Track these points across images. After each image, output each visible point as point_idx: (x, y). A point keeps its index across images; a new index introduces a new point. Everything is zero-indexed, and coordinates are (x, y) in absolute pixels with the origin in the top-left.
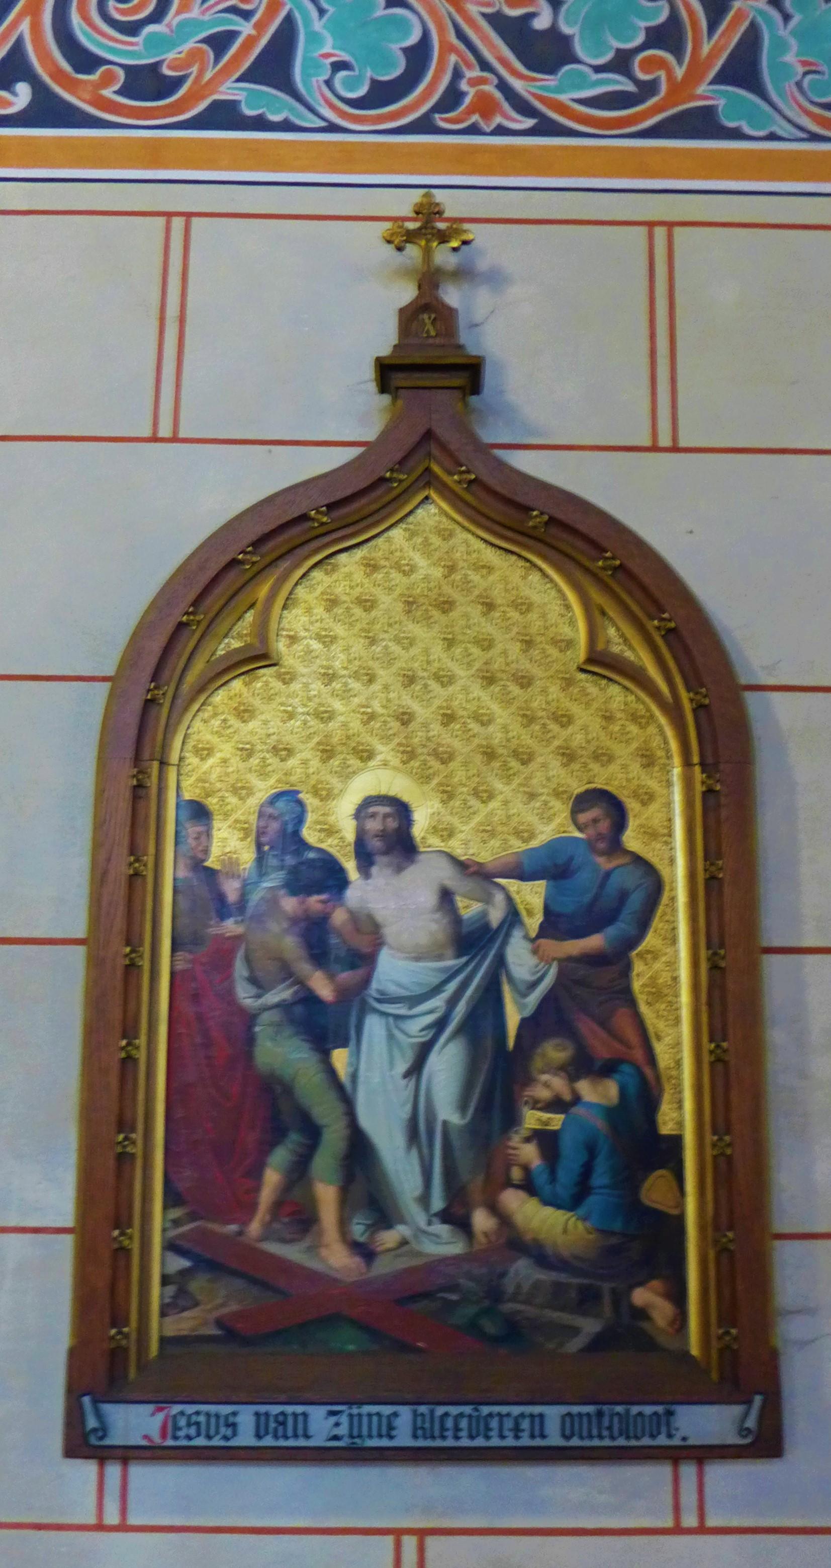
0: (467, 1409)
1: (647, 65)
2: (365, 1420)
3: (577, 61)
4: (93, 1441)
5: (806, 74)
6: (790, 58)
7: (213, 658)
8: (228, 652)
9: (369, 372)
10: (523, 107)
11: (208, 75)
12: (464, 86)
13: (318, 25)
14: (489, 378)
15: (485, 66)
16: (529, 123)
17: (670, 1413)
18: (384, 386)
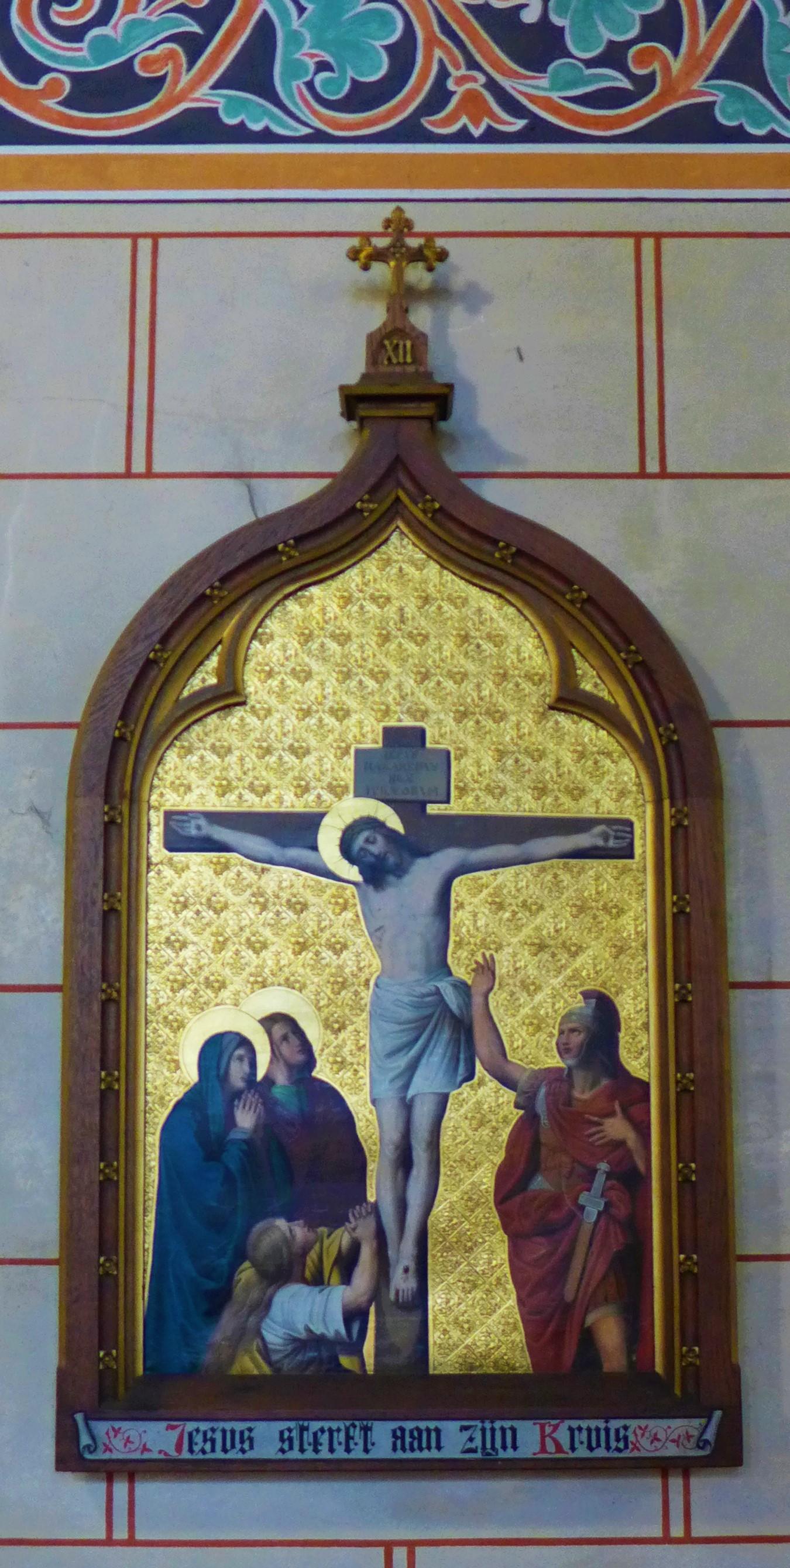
1: (642, 59)
2: (498, 1435)
9: (335, 404)
12: (451, 85)
14: (459, 406)
16: (520, 124)
17: (366, 1430)
18: (349, 413)
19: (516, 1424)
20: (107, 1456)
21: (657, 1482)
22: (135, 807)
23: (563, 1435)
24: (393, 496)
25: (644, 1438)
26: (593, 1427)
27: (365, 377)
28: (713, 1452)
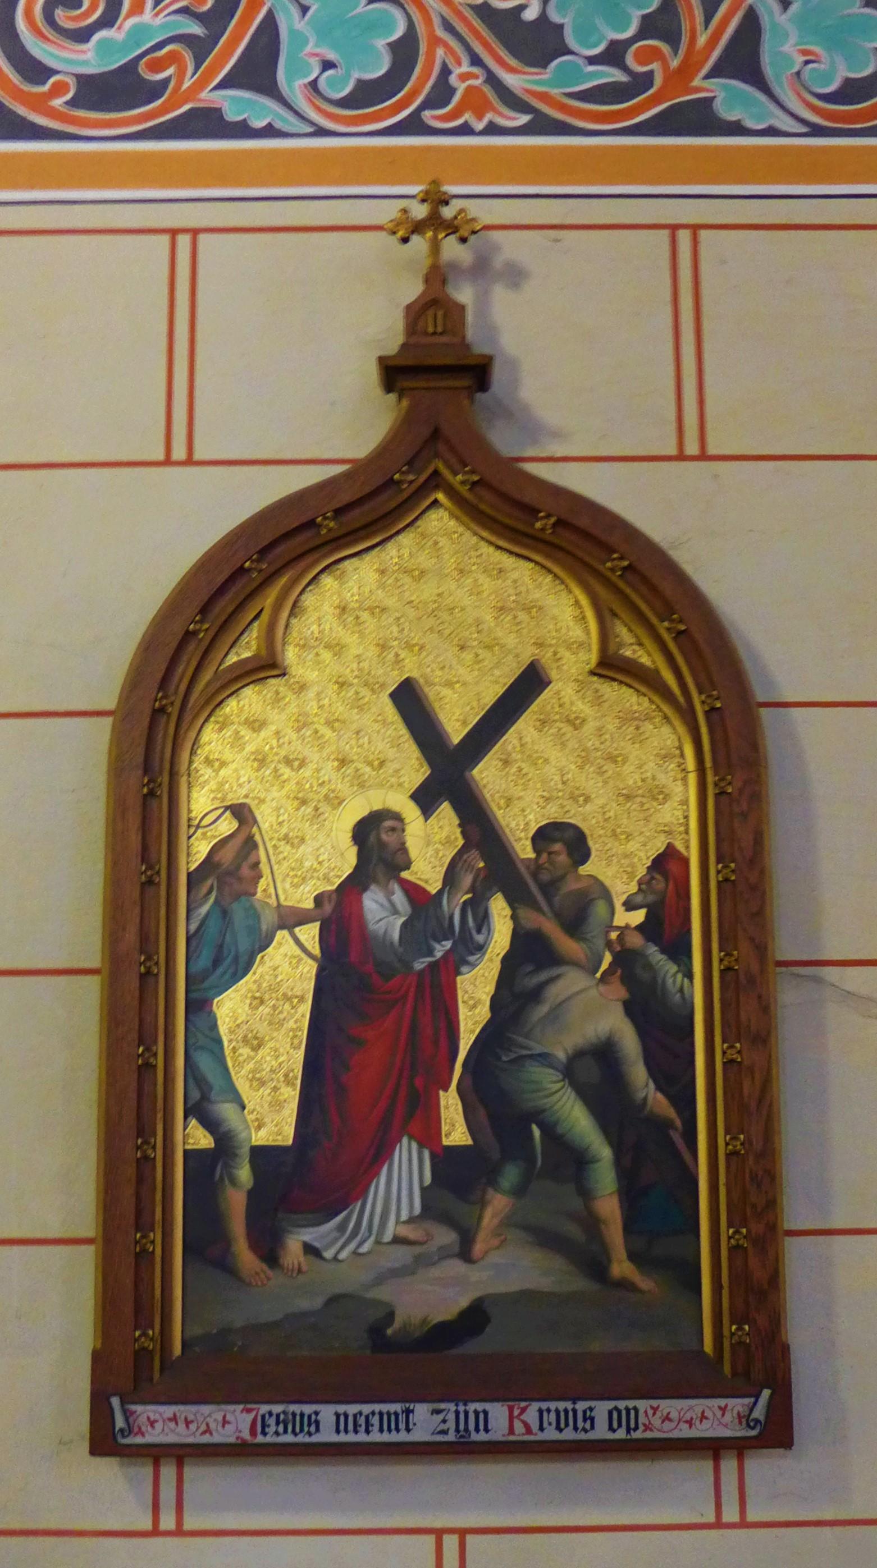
3: (570, 52)
5: (807, 62)
6: (788, 47)
7: (222, 668)
9: (373, 373)
11: (187, 84)
14: (498, 375)
16: (524, 119)
17: (408, 1412)
19: (488, 1406)
23: (531, 1416)
24: (429, 471)
27: (404, 346)
28: (760, 1434)
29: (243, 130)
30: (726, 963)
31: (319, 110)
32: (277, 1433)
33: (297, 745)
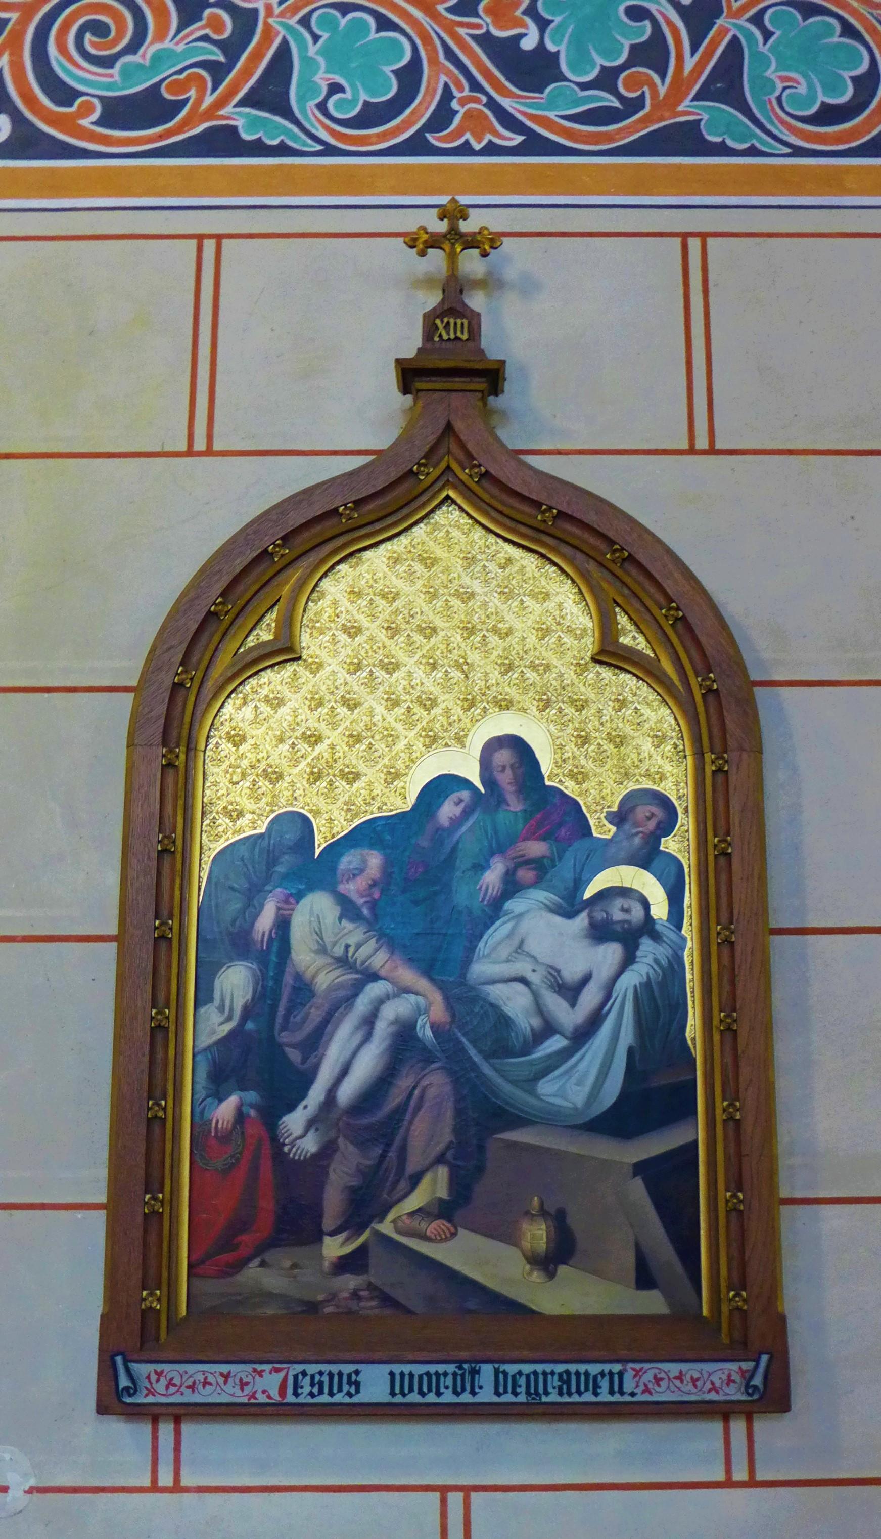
0: (451, 1368)
4: (129, 1400)
5: (785, 88)
7: (242, 650)
8: (259, 644)
9: (391, 377)
10: (509, 121)
12: (454, 105)
13: (312, 50)
15: (475, 86)
16: (519, 139)
18: (405, 388)
20: (150, 1399)
21: (717, 1427)
22: (192, 753)
24: (443, 465)
25: (228, 1385)
26: (406, 1371)
29: (258, 148)
30: (722, 936)
31: (327, 128)
32: (312, 1395)
33: (312, 723)
